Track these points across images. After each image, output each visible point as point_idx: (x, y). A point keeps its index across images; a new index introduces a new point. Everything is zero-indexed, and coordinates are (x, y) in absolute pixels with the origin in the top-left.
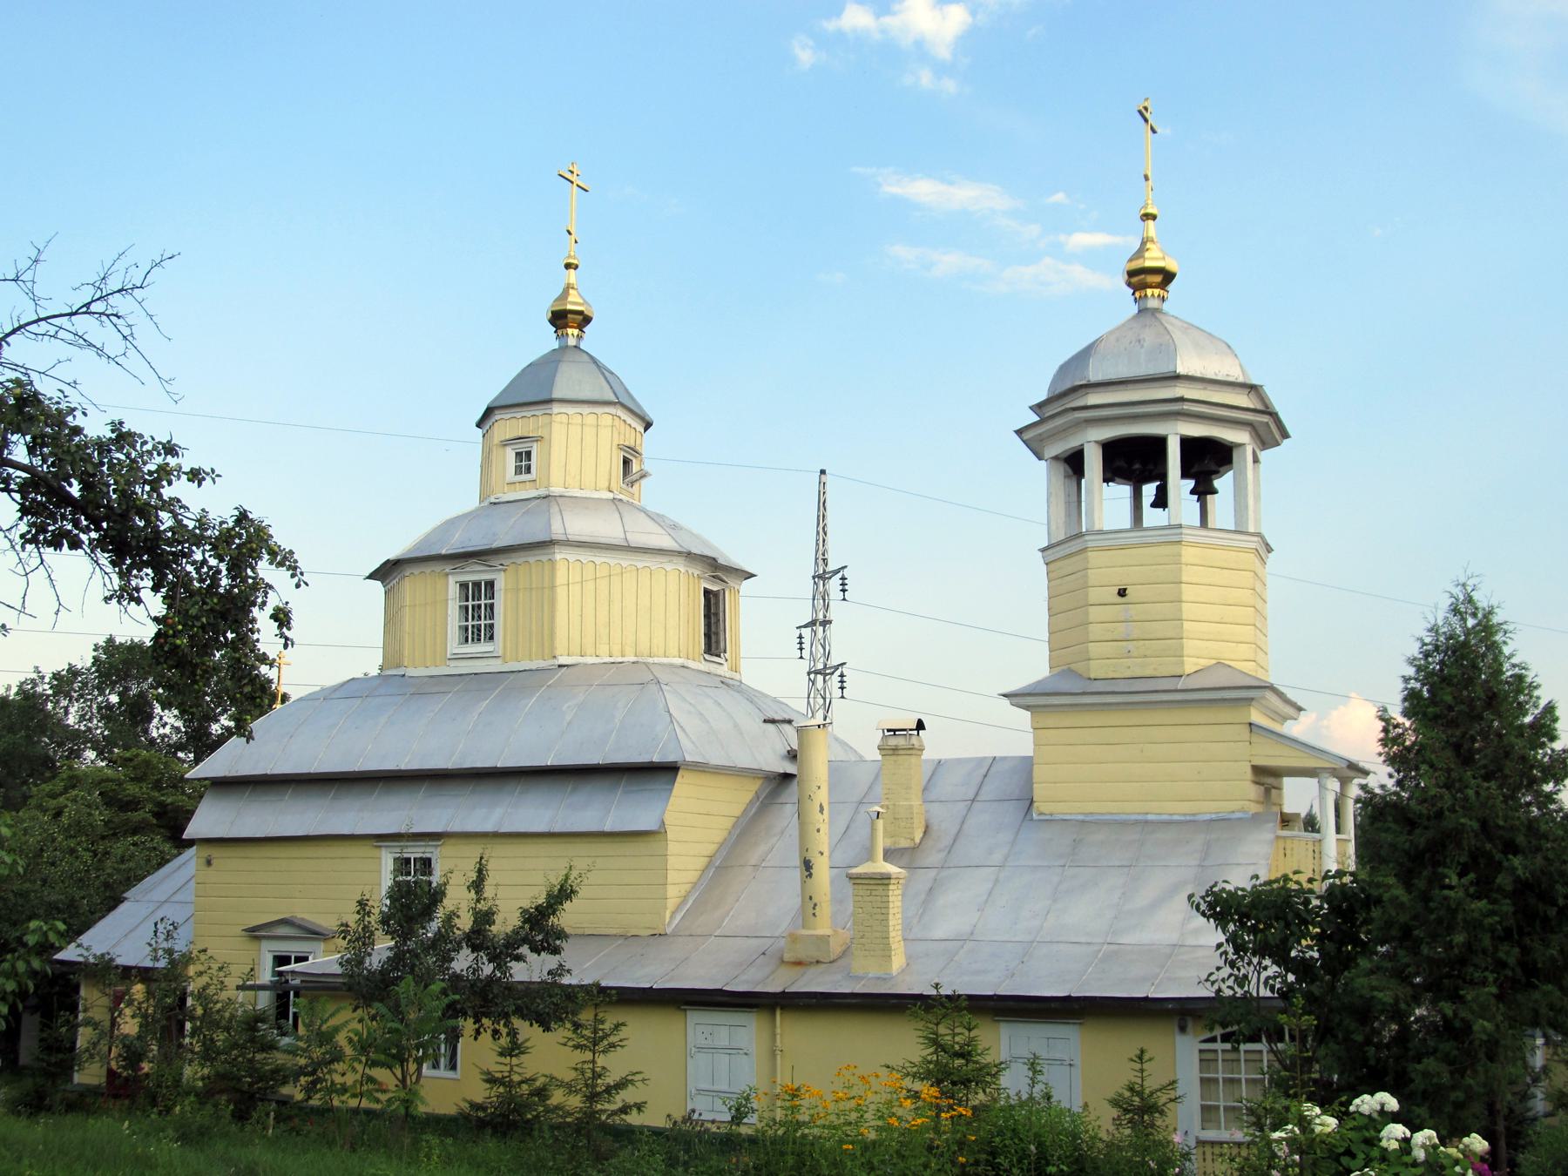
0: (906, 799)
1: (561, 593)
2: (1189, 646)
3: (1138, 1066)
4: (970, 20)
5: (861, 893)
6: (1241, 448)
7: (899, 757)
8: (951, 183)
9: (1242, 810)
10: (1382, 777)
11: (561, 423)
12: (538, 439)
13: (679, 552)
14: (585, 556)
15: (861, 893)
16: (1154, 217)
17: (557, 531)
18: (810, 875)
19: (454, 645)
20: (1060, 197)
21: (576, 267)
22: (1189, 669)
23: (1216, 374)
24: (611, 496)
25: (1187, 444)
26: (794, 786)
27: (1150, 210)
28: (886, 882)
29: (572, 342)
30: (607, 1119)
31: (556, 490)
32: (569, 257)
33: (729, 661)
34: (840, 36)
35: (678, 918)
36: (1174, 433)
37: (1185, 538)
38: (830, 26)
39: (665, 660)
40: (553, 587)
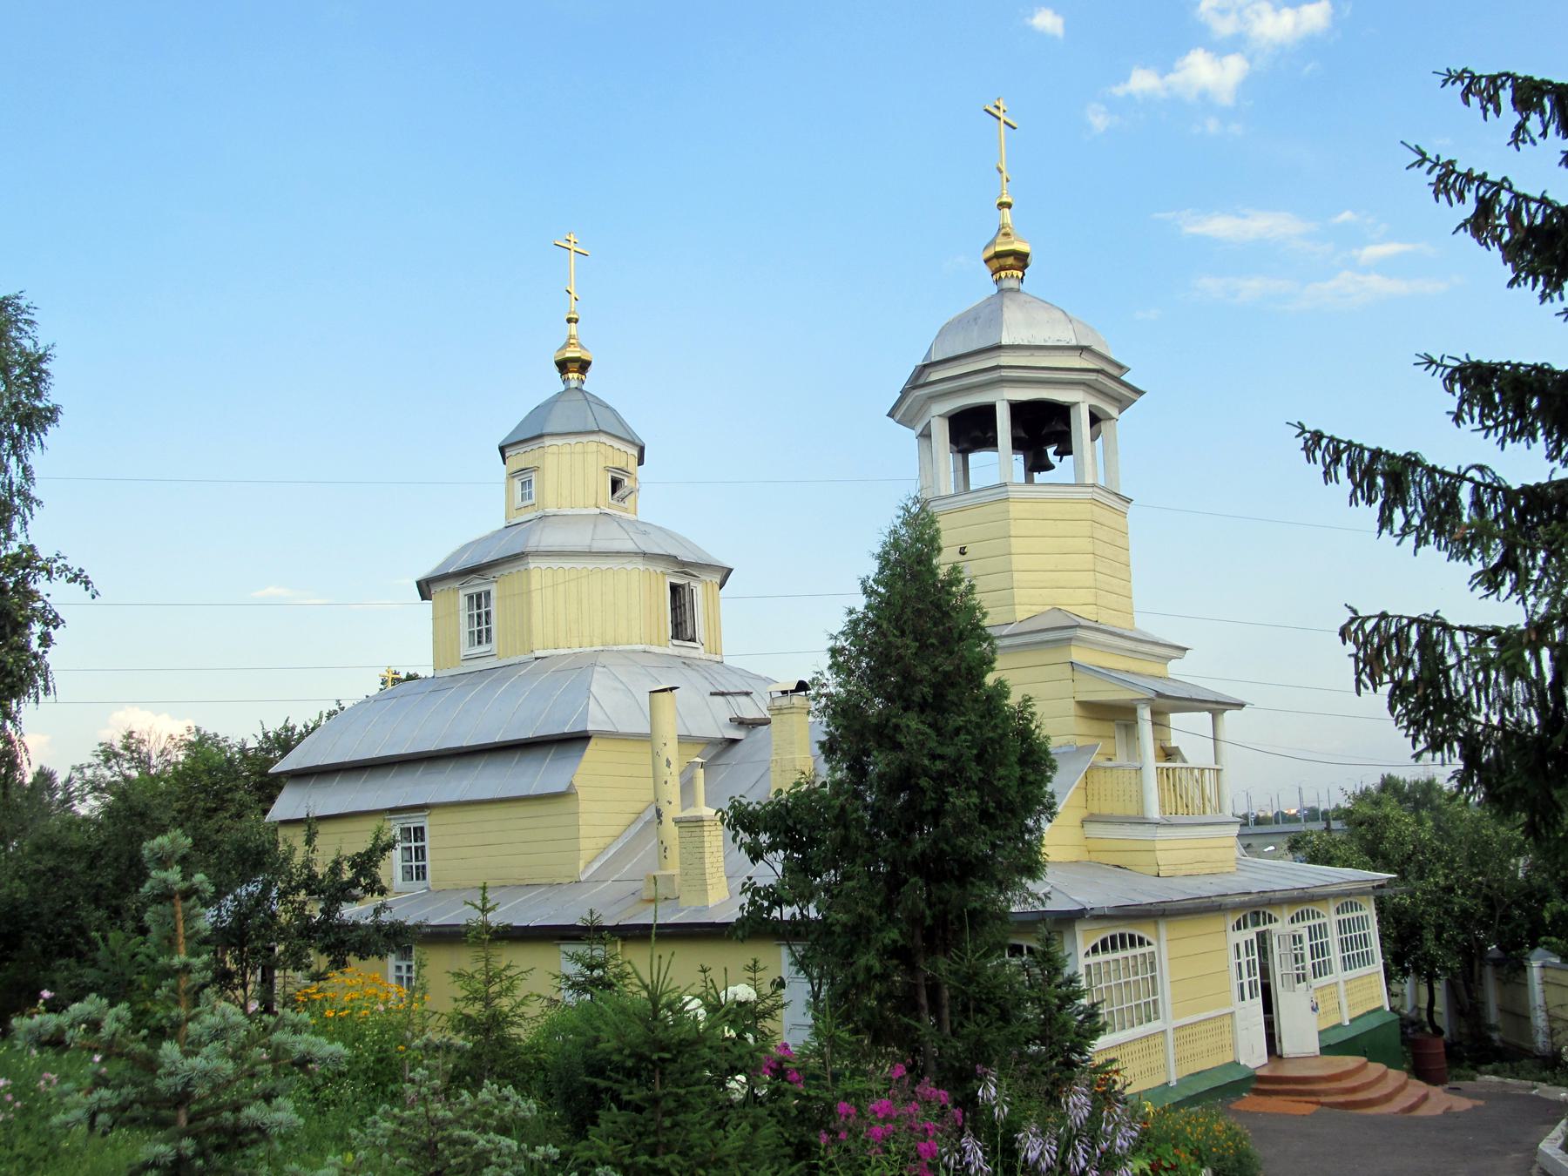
0: (791, 753)
1: (536, 597)
2: (1020, 595)
3: (752, 975)
4: (1247, 66)
5: (685, 834)
6: (1076, 407)
7: (786, 716)
8: (1245, 217)
9: (1068, 744)
10: (833, 685)
11: (553, 454)
12: (536, 469)
13: (636, 553)
14: (555, 563)
15: (685, 834)
16: (1009, 206)
17: (532, 545)
18: (661, 822)
19: (465, 650)
20: (1346, 216)
21: (576, 321)
22: (1020, 617)
23: (1045, 341)
24: (598, 511)
25: (1017, 409)
26: (738, 747)
27: (1005, 199)
28: (700, 824)
29: (574, 384)
30: (1383, 1076)
31: (551, 510)
32: (570, 313)
33: (706, 645)
34: (1130, 97)
35: (596, 866)
36: (1002, 401)
37: (1011, 495)
38: (1119, 91)
39: (628, 647)
40: (529, 592)
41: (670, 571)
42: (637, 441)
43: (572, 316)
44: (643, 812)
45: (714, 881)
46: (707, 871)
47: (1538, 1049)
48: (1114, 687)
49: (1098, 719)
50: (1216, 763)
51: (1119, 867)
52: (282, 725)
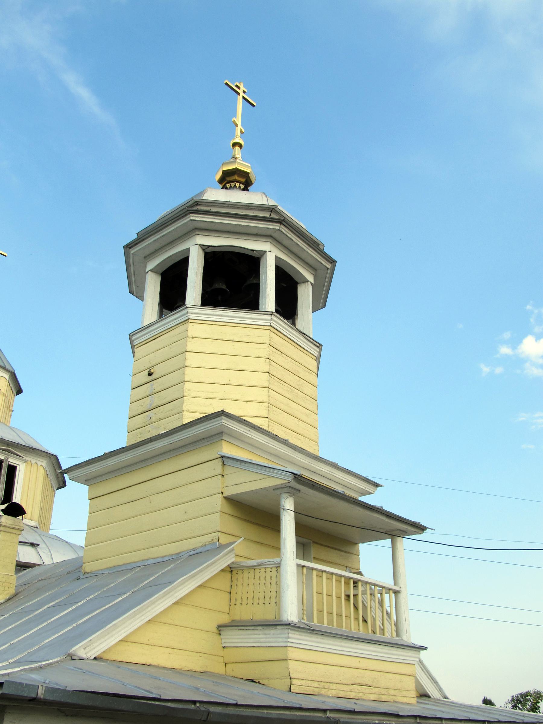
42: (8, 367)
47: (132, 339)
48: (261, 476)
49: (257, 524)
50: (395, 584)
51: (252, 681)
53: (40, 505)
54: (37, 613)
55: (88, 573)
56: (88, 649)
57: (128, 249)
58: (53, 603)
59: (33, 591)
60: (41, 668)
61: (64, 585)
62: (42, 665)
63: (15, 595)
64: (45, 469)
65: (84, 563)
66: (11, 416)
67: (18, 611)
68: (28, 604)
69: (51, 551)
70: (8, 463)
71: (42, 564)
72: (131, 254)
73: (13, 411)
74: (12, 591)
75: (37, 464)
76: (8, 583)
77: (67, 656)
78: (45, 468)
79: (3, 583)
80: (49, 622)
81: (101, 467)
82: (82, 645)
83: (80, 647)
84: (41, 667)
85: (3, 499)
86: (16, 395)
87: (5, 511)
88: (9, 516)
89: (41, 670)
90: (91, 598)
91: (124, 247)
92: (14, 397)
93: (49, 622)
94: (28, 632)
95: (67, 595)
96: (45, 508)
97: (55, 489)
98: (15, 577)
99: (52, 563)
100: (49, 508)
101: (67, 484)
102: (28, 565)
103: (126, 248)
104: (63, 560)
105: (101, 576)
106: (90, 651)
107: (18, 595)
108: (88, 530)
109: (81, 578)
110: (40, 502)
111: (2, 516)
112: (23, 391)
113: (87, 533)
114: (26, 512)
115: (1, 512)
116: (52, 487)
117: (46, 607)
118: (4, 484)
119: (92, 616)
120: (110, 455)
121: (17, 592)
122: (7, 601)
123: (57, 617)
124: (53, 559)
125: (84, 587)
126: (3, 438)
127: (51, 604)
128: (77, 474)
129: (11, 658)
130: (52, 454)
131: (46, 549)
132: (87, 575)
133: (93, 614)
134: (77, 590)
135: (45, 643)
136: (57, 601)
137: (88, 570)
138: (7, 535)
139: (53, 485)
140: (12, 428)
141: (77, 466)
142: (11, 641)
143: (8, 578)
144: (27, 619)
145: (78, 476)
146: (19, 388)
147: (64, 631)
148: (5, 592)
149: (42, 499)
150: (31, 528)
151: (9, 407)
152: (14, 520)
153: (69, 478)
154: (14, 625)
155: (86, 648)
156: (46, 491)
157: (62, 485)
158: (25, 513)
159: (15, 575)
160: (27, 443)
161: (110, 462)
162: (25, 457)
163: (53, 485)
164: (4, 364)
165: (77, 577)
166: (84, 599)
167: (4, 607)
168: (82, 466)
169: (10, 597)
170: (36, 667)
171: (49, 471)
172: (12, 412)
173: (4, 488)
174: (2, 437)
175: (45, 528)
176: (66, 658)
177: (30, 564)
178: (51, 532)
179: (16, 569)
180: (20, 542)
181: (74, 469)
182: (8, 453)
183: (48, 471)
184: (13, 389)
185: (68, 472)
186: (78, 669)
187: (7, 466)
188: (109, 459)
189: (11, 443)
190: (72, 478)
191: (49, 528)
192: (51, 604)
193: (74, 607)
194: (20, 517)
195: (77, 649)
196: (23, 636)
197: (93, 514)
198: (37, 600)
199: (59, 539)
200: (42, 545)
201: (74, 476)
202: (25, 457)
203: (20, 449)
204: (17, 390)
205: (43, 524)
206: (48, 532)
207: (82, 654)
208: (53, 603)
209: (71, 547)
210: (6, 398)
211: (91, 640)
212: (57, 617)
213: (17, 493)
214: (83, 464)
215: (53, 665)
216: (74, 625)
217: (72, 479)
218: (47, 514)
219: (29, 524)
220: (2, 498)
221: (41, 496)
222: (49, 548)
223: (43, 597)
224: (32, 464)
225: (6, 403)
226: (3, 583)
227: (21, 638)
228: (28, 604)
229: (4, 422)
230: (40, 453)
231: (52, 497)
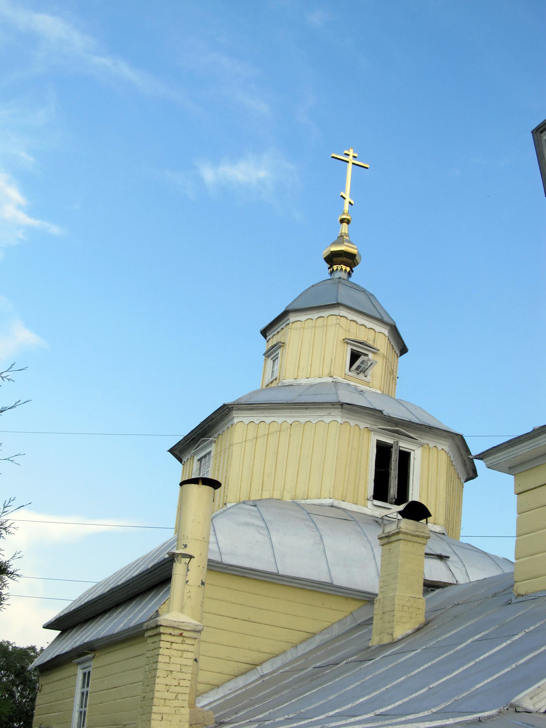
41: (375, 427)
42: (386, 319)
43: (344, 217)
44: (260, 664)
45: (166, 710)
46: (157, 694)
52: (201, 633)
53: (445, 504)
54: (458, 648)
55: (522, 595)
56: (535, 699)
57: (538, 134)
58: (479, 636)
59: (449, 619)
60: (480, 721)
61: (490, 612)
62: (481, 717)
63: (426, 624)
64: (448, 454)
65: (516, 582)
66: (395, 384)
67: (433, 645)
68: (445, 636)
69: (466, 566)
70: (399, 449)
71: (455, 583)
72: (544, 141)
73: (398, 378)
74: (421, 619)
75: (437, 449)
76: (416, 608)
77: (510, 707)
78: (447, 452)
79: (409, 608)
80: (477, 660)
81: (530, 448)
82: (528, 694)
83: (526, 695)
84: (480, 720)
85: (396, 497)
86: (400, 356)
87: (403, 514)
88: (410, 520)
89: (480, 724)
90: (531, 630)
91: (532, 132)
92: (397, 359)
93: (477, 660)
94: (451, 673)
95: (497, 626)
96: (452, 507)
97: (463, 481)
98: (423, 600)
99: (469, 582)
100: (457, 508)
101: (478, 474)
102: (437, 585)
103: (536, 133)
104: (484, 578)
105: (542, 600)
106: (539, 701)
107: (430, 625)
108: (517, 537)
109: (512, 602)
110: (445, 499)
111: (401, 519)
112: (409, 350)
113: (516, 540)
114: (432, 511)
115: (399, 515)
116: (458, 478)
117: (470, 641)
118: (396, 476)
119: (536, 655)
120: (542, 431)
121: (428, 620)
122: (415, 632)
123: (487, 654)
124: (468, 576)
125: (520, 615)
126: (390, 415)
127: (476, 637)
128: (497, 460)
129: (434, 707)
130: (455, 433)
131: (459, 563)
132: (521, 599)
133: (538, 651)
134: (510, 618)
135: (476, 688)
136: (483, 633)
137: (522, 591)
138: (409, 545)
139: (461, 476)
140: (398, 401)
141: (496, 449)
142: (431, 684)
143: (415, 602)
144: (447, 656)
145: (498, 462)
146: (403, 345)
147: (500, 673)
148: (413, 620)
149: (447, 495)
150: (436, 535)
151: (392, 372)
152: (417, 525)
153: (487, 465)
154: (430, 664)
155: (533, 697)
156: (451, 485)
157: (471, 474)
158: (430, 515)
159: (423, 598)
160: (421, 420)
161: (542, 441)
162: (420, 440)
163: (461, 476)
164: (379, 313)
165: (508, 602)
166: (522, 631)
167: (413, 639)
168: (503, 448)
169: (420, 627)
170: (474, 719)
171: (454, 457)
172: (397, 380)
173: (397, 483)
174: (388, 414)
175: (454, 534)
176: (507, 709)
177: (439, 584)
178: (462, 540)
179: (424, 590)
180: (426, 554)
181: (491, 453)
182: (399, 435)
183: (452, 457)
184: (395, 348)
185: (484, 457)
186: (527, 724)
187: (398, 453)
188: (540, 437)
189: (401, 421)
190: (490, 465)
191: (460, 535)
192: (476, 637)
193: (509, 642)
194: (424, 521)
195: (522, 698)
196: (445, 679)
197: (523, 514)
198: (456, 631)
199: (480, 552)
200: (453, 558)
201: (492, 463)
202: (420, 440)
203: (412, 429)
204: (401, 349)
205: (451, 529)
206: (458, 540)
207: (528, 705)
208: (479, 636)
209: (493, 560)
210: (387, 360)
211: (539, 687)
212: (487, 654)
213: (414, 488)
214: (504, 446)
215: (494, 719)
216: (513, 666)
217: (491, 467)
218: (455, 515)
219: (433, 530)
220: (395, 496)
221: (445, 492)
222: (463, 561)
223: (463, 627)
224: (430, 448)
225: (388, 367)
226: (409, 608)
227: (442, 681)
228: (445, 636)
229: (388, 394)
230: (440, 433)
231: (460, 492)
